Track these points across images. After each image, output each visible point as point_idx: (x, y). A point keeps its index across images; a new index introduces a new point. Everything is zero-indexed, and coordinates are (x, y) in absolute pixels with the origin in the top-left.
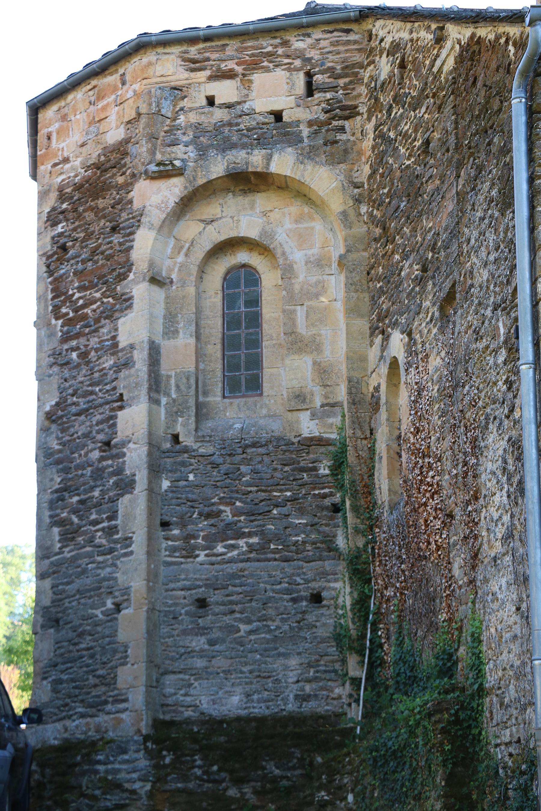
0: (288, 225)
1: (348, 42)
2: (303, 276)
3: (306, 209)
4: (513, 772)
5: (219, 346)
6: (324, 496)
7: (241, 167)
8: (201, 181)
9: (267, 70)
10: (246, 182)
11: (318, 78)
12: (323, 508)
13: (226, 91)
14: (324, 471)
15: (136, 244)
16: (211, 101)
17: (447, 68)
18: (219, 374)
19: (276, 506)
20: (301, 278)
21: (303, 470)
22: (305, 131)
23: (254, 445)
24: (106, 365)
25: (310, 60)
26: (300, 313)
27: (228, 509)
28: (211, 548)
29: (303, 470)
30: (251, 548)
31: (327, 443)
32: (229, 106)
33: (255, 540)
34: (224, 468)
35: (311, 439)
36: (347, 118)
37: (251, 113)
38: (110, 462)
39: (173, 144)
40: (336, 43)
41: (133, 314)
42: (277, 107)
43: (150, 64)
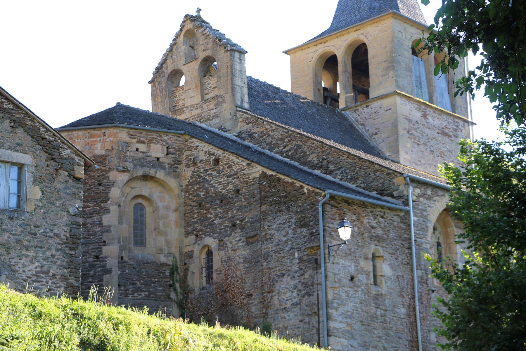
0: (157, 194)
1: (180, 141)
2: (162, 211)
3: (163, 190)
4: (386, 234)
5: (133, 229)
6: (167, 282)
7: (147, 173)
8: (135, 176)
9: (155, 144)
10: (146, 178)
11: (171, 150)
12: (167, 285)
13: (142, 147)
14: (167, 273)
15: (111, 192)
16: (137, 150)
17: (254, 175)
18: (133, 238)
19: (153, 283)
20: (161, 211)
21: (161, 273)
22: (167, 166)
23: (147, 263)
24: (97, 230)
25: (168, 143)
26: (161, 223)
27: (139, 282)
28: (133, 294)
29: (161, 273)
30: (146, 296)
31: (169, 265)
32: (143, 153)
33: (147, 293)
34: (137, 269)
35: (164, 263)
36: (179, 164)
37: (150, 156)
38: (99, 263)
39: (126, 161)
40: (176, 140)
41: (110, 215)
42: (158, 156)
43: (117, 133)
